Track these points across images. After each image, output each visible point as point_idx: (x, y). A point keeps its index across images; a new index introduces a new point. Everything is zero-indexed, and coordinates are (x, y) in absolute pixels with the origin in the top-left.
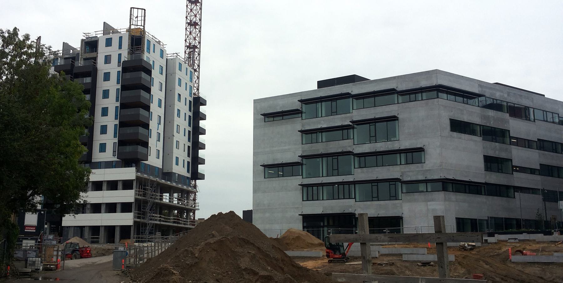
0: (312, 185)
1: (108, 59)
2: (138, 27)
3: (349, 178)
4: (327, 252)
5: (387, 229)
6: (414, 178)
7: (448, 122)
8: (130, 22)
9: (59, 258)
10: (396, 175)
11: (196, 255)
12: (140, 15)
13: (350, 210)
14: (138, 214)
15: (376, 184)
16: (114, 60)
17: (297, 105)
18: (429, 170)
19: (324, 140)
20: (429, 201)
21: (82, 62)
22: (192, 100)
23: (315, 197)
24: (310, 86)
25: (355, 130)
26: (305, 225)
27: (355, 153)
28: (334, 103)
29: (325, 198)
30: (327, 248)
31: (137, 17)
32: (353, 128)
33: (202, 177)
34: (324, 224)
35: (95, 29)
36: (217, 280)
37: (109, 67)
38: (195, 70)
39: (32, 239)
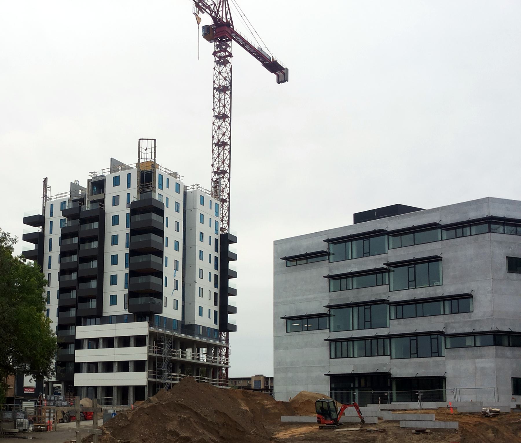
0: (341, 340)
1: (116, 201)
2: (148, 160)
3: (384, 332)
4: (318, 418)
5: (419, 391)
6: (460, 331)
7: (505, 261)
8: (139, 157)
9: (52, 420)
10: (439, 328)
11: (129, 418)
12: (149, 146)
13: (385, 370)
14: (154, 373)
15: (415, 338)
16: (123, 201)
17: (323, 247)
18: (478, 320)
19: (355, 287)
20: (477, 358)
21: (89, 206)
22: (218, 237)
23: (345, 354)
24: (342, 221)
25: (391, 274)
26: (333, 386)
27: (390, 301)
28: (366, 242)
29: (356, 355)
30: (318, 413)
31: (147, 149)
32: (389, 271)
33: (234, 328)
34: (354, 385)
35: (102, 168)
36: (143, 440)
37: (117, 211)
38: (223, 201)
39: (31, 401)
